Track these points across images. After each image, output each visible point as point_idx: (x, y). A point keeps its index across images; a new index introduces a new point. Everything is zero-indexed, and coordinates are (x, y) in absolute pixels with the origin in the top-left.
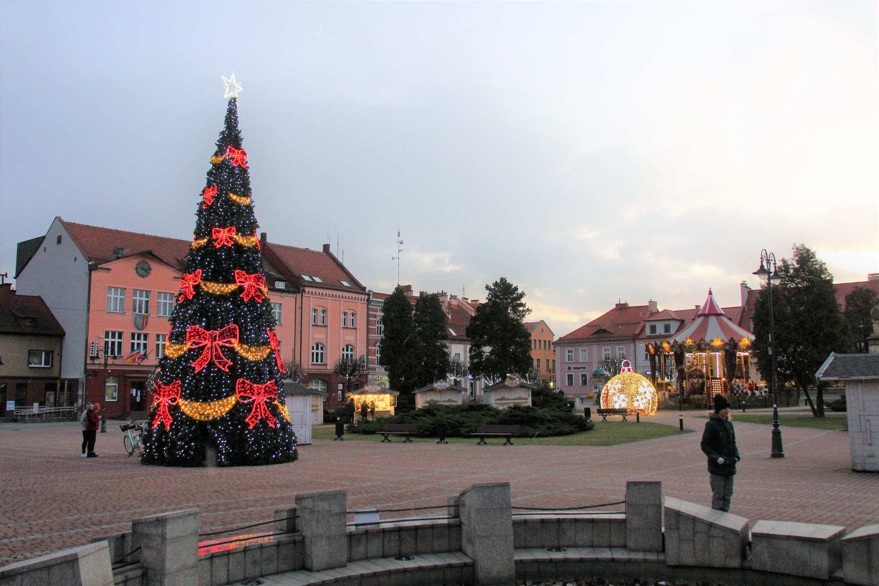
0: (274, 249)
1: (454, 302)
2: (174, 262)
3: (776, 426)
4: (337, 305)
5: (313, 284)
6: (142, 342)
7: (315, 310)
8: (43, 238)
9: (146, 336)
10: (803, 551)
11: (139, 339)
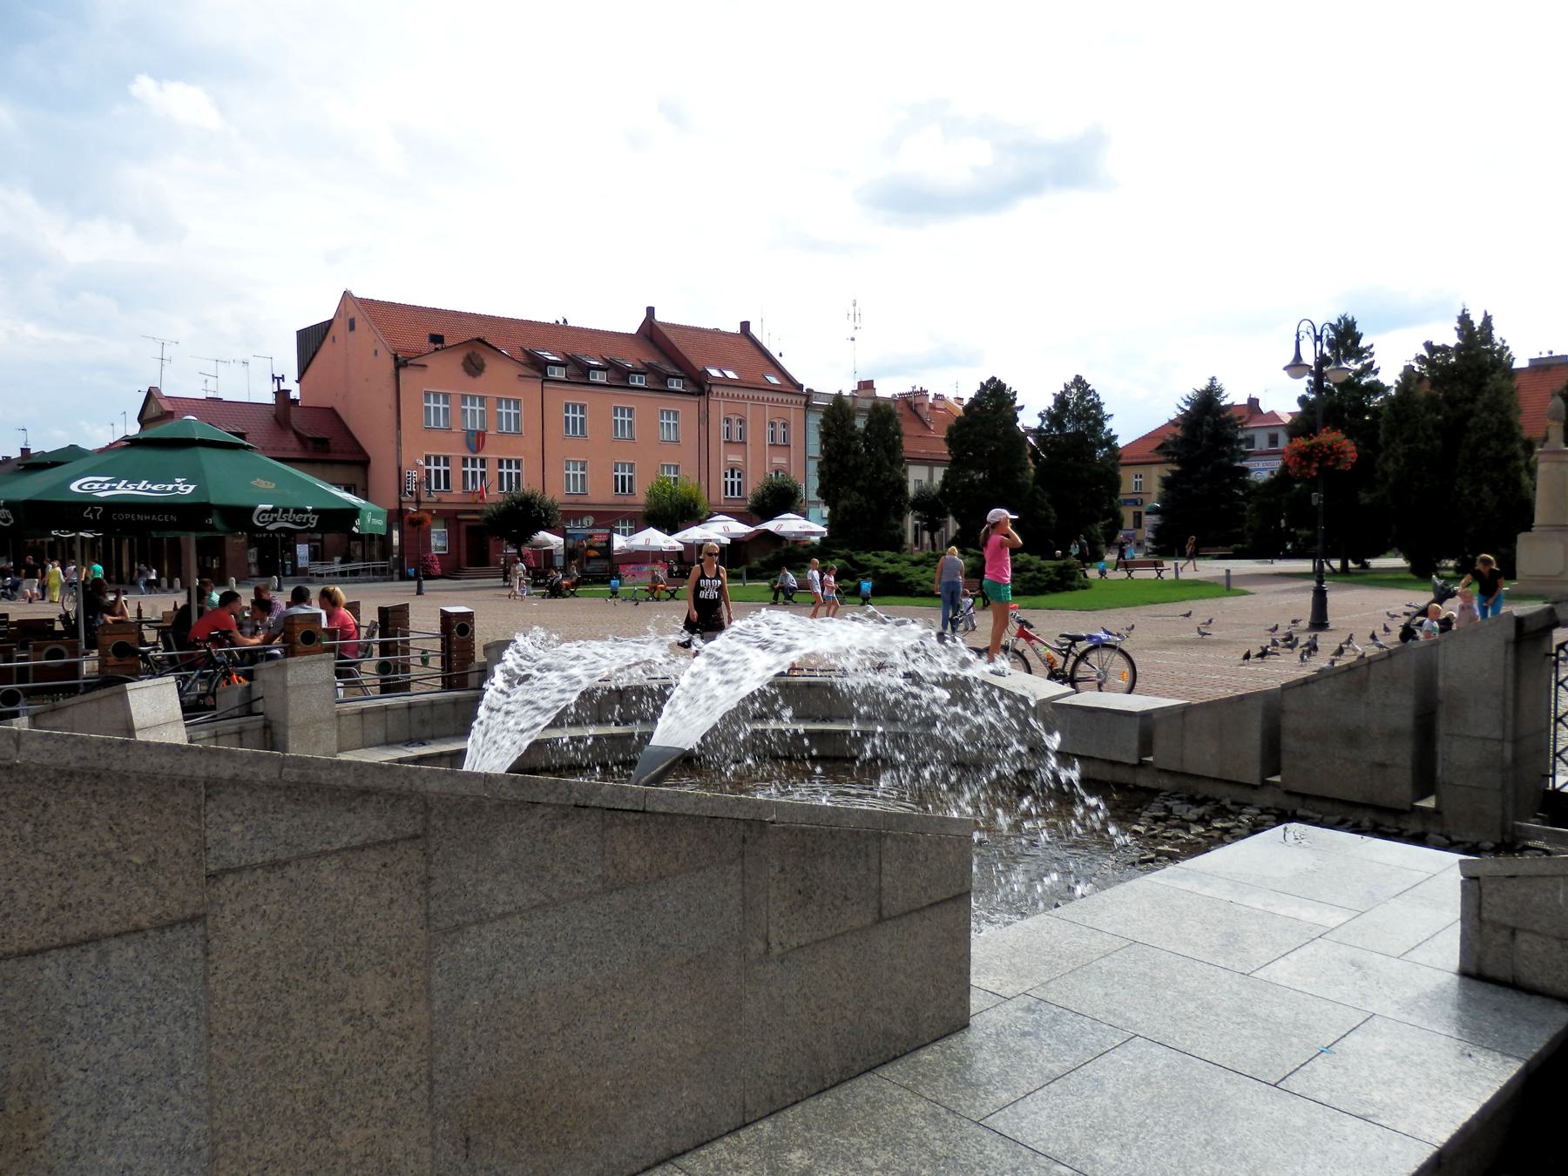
0: (664, 330)
1: (940, 405)
2: (520, 356)
3: (1320, 582)
4: (759, 416)
5: (725, 383)
6: (479, 469)
7: (773, 424)
8: (330, 322)
9: (483, 462)
10: (166, 761)
11: (437, 464)
